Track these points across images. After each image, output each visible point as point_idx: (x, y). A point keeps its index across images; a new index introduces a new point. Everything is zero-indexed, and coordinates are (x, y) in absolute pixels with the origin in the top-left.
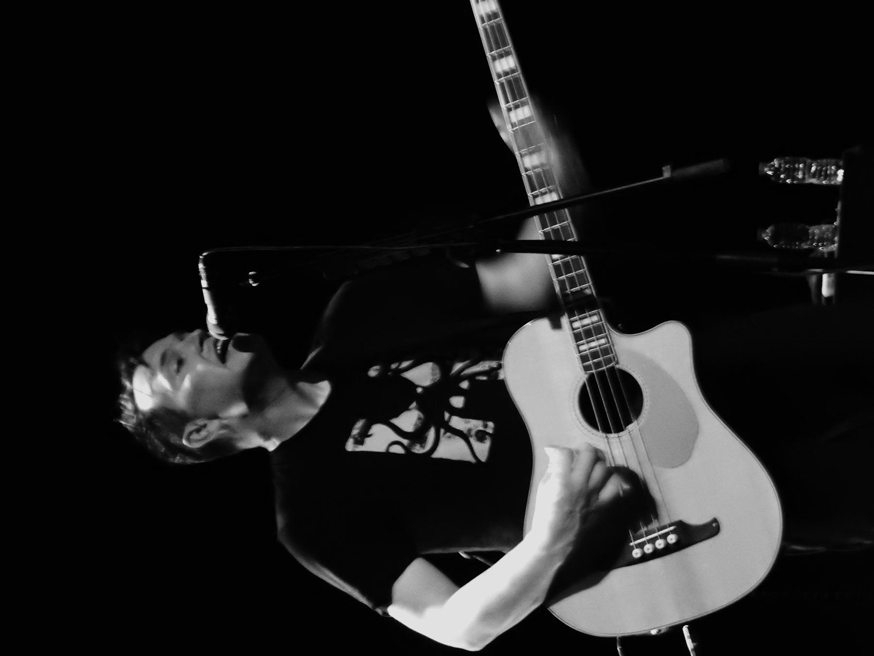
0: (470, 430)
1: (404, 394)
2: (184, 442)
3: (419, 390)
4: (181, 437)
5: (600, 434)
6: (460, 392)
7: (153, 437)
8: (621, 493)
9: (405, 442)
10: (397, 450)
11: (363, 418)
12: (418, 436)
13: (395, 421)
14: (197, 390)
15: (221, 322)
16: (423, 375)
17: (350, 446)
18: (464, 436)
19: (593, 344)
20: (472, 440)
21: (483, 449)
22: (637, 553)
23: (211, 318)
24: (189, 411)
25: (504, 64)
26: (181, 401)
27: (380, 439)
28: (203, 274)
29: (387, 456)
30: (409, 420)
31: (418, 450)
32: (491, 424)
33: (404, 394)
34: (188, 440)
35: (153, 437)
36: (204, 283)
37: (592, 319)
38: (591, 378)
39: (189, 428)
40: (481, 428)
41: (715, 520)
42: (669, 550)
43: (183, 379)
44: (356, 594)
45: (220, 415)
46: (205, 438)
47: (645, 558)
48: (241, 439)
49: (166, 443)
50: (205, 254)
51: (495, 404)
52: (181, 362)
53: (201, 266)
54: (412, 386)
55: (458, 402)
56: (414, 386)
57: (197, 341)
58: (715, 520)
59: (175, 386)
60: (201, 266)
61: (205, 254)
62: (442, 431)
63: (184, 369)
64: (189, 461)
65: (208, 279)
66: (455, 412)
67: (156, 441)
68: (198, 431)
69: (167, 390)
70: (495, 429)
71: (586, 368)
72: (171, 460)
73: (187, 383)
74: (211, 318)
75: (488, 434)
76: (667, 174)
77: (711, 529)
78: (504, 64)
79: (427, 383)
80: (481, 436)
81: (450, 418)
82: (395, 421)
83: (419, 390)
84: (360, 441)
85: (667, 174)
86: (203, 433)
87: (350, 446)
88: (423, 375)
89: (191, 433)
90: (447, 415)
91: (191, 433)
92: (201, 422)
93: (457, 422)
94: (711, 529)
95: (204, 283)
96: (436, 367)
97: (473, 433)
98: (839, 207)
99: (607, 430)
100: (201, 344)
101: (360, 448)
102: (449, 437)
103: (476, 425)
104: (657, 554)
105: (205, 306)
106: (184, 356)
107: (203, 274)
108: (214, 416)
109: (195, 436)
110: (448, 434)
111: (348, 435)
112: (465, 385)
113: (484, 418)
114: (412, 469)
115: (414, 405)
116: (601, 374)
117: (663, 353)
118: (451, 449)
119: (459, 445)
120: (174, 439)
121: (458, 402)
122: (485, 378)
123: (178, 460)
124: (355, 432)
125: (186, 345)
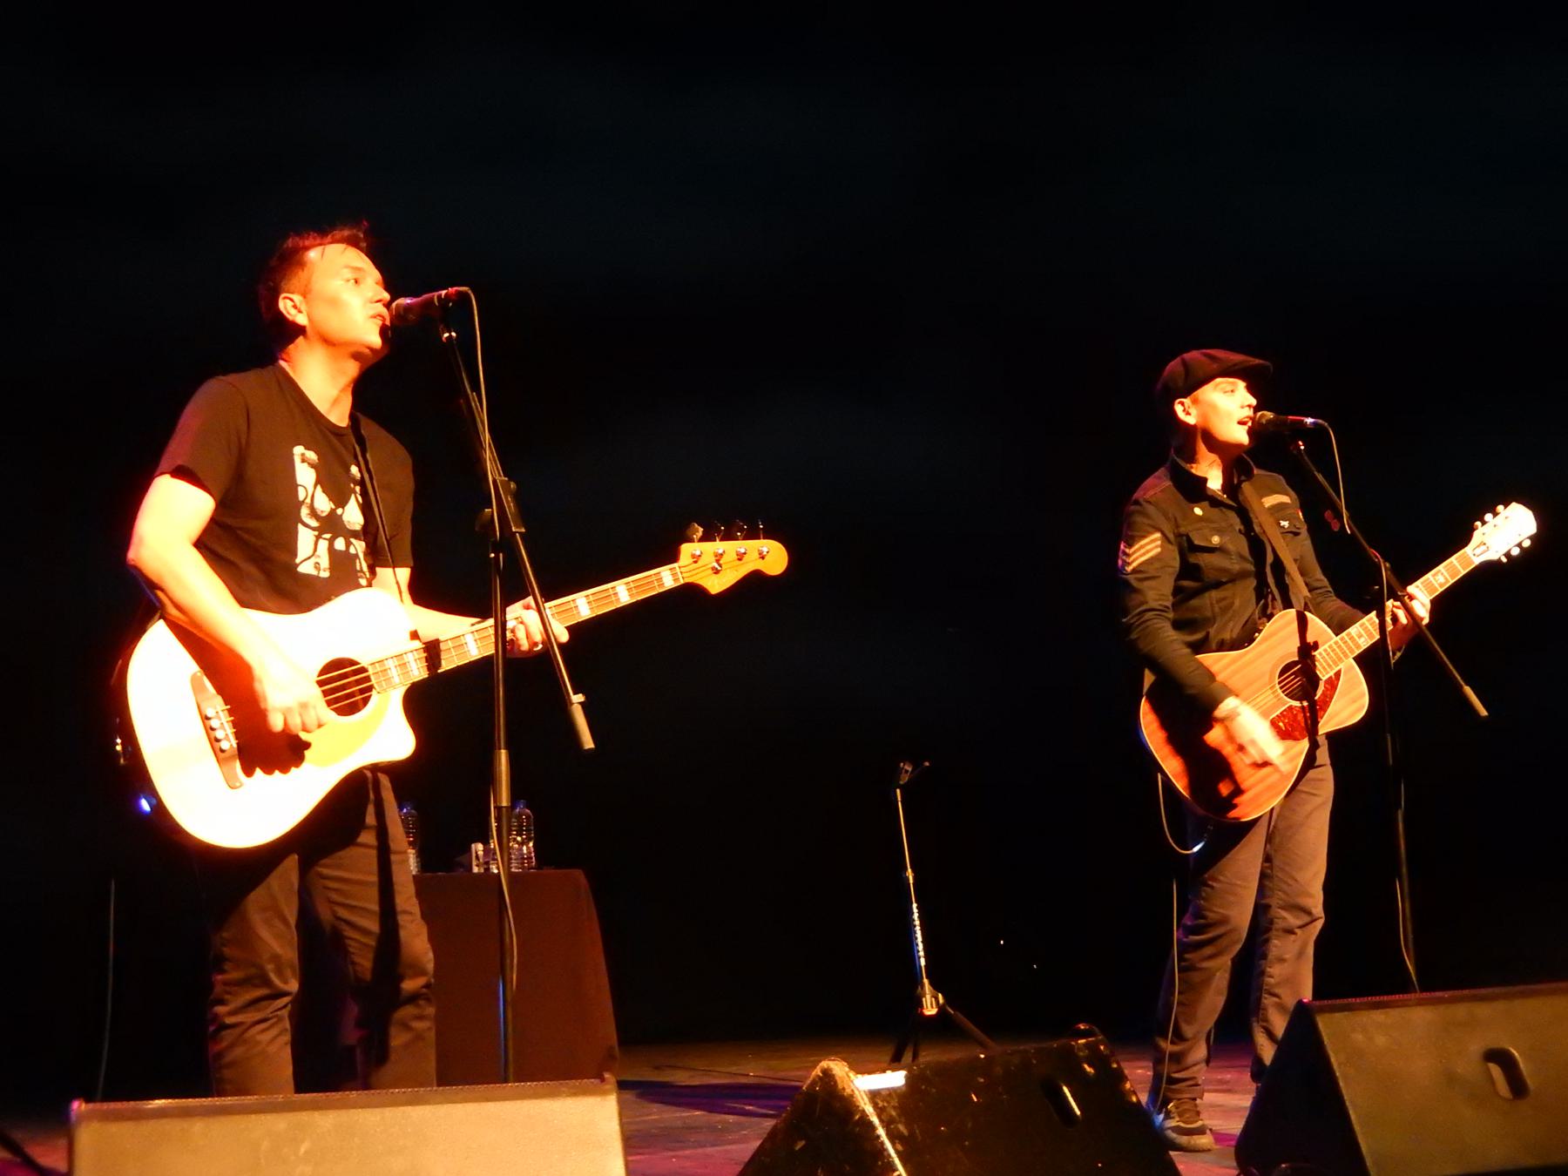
1: (340, 500)
3: (339, 511)
5: (374, 692)
6: (348, 544)
8: (1232, 898)
10: (301, 495)
12: (314, 513)
17: (298, 450)
20: (313, 560)
25: (666, 578)
27: (305, 476)
29: (293, 486)
30: (324, 504)
31: (304, 512)
38: (363, 670)
51: (343, 577)
66: (331, 542)
68: (295, 307)
78: (666, 578)
79: (345, 518)
85: (577, 698)
86: (293, 311)
87: (298, 450)
88: (353, 516)
90: (328, 536)
92: (303, 308)
93: (323, 545)
98: (714, 563)
101: (297, 460)
103: (325, 561)
111: (307, 448)
114: (287, 514)
116: (368, 679)
119: (311, 555)
121: (340, 544)
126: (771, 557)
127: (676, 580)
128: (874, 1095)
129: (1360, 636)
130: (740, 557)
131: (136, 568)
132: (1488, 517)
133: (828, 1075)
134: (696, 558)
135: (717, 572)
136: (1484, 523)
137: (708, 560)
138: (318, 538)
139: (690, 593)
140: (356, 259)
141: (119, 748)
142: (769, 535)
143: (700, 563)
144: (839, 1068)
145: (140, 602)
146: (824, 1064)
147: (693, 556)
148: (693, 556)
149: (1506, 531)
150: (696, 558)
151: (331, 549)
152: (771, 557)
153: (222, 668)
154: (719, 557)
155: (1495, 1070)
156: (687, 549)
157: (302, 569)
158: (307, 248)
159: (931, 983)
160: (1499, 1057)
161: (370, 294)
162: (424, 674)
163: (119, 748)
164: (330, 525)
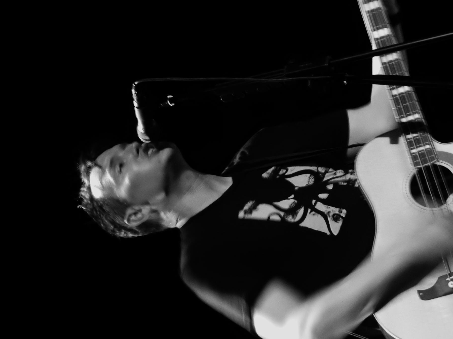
0: (329, 212)
1: (286, 190)
2: (126, 222)
3: (293, 196)
4: (123, 218)
6: (325, 191)
7: (104, 218)
9: (282, 214)
11: (253, 200)
12: (292, 211)
14: (135, 186)
15: (147, 131)
16: (301, 181)
17: (241, 215)
18: (324, 216)
20: (329, 219)
21: (336, 227)
23: (140, 128)
24: (129, 200)
26: (122, 192)
27: (264, 212)
28: (135, 97)
29: (268, 222)
30: (286, 204)
31: (290, 219)
32: (344, 211)
33: (286, 190)
34: (129, 221)
35: (104, 218)
36: (135, 104)
38: (420, 171)
39: (129, 211)
40: (337, 212)
43: (123, 178)
45: (150, 202)
46: (141, 219)
49: (113, 223)
50: (136, 83)
52: (121, 165)
53: (133, 91)
54: (292, 186)
55: (323, 196)
56: (293, 186)
57: (135, 151)
59: (118, 182)
60: (133, 91)
61: (136, 83)
62: (309, 210)
63: (124, 170)
64: (130, 235)
65: (139, 101)
67: (106, 221)
68: (135, 214)
69: (110, 183)
70: (347, 215)
71: (416, 164)
72: (118, 234)
73: (127, 181)
74: (140, 128)
75: (342, 217)
80: (336, 218)
81: (316, 203)
83: (296, 188)
84: (250, 211)
86: (139, 215)
87: (241, 215)
89: (130, 216)
90: (314, 201)
91: (130, 216)
92: (137, 208)
93: (320, 206)
95: (135, 104)
96: (312, 177)
97: (331, 214)
100: (138, 151)
101: (249, 216)
102: (314, 215)
103: (334, 210)
105: (137, 119)
106: (125, 161)
107: (135, 97)
108: (146, 203)
109: (133, 218)
110: (313, 212)
111: (242, 208)
112: (330, 187)
113: (340, 207)
114: (286, 232)
115: (293, 196)
116: (427, 168)
118: (313, 222)
120: (118, 220)
122: (345, 184)
123: (123, 234)
124: (246, 207)
125: (126, 153)
131: (90, 172)
138: (314, 209)
149: (265, 175)
151: (324, 201)
152: (247, 153)
157: (335, 233)
158: (92, 198)
159: (222, 289)
161: (131, 156)
162: (318, 203)
163: (169, 97)
164: (305, 198)
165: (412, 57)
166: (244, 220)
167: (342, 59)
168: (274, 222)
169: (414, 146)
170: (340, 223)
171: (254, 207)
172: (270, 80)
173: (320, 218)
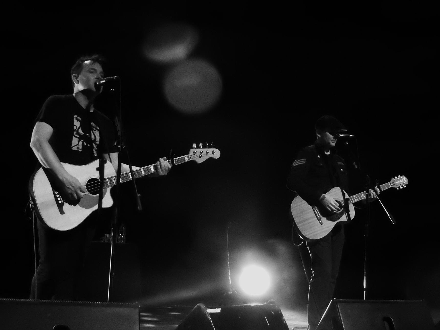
12: (78, 133)
13: (132, 167)
18: (78, 145)
19: (114, 181)
21: (75, 148)
22: (56, 193)
27: (77, 124)
29: (73, 125)
30: (80, 131)
31: (75, 133)
37: (114, 182)
41: (64, 213)
42: (57, 201)
44: (389, 215)
47: (55, 195)
48: (169, 168)
55: (85, 144)
58: (64, 213)
76: (138, 195)
77: (62, 212)
80: (78, 148)
82: (132, 167)
84: (77, 119)
85: (138, 195)
87: (75, 116)
93: (81, 143)
94: (62, 212)
99: (87, 186)
101: (75, 119)
104: (56, 198)
113: (82, 149)
114: (70, 132)
116: (87, 189)
117: (108, 201)
118: (75, 141)
119: (76, 144)
126: (216, 154)
127: (189, 159)
128: (212, 314)
129: (356, 198)
130: (207, 153)
132: (396, 177)
133: (199, 308)
134: (195, 153)
135: (200, 157)
136: (394, 178)
137: (198, 154)
139: (192, 163)
140: (98, 68)
141: (356, 167)
142: (215, 147)
143: (196, 155)
144: (202, 306)
145: (35, 165)
146: (198, 304)
147: (194, 152)
148: (194, 152)
149: (401, 181)
150: (195, 153)
151: (83, 144)
152: (216, 154)
153: (57, 184)
154: (201, 153)
155: (386, 324)
156: (192, 151)
160: (388, 320)
163: (356, 167)
165: (130, 182)
166: (73, 117)
167: (172, 313)
168: (74, 127)
169: (37, 299)
170: (76, 150)
171: (78, 120)
172: (146, 314)
173: (77, 143)
